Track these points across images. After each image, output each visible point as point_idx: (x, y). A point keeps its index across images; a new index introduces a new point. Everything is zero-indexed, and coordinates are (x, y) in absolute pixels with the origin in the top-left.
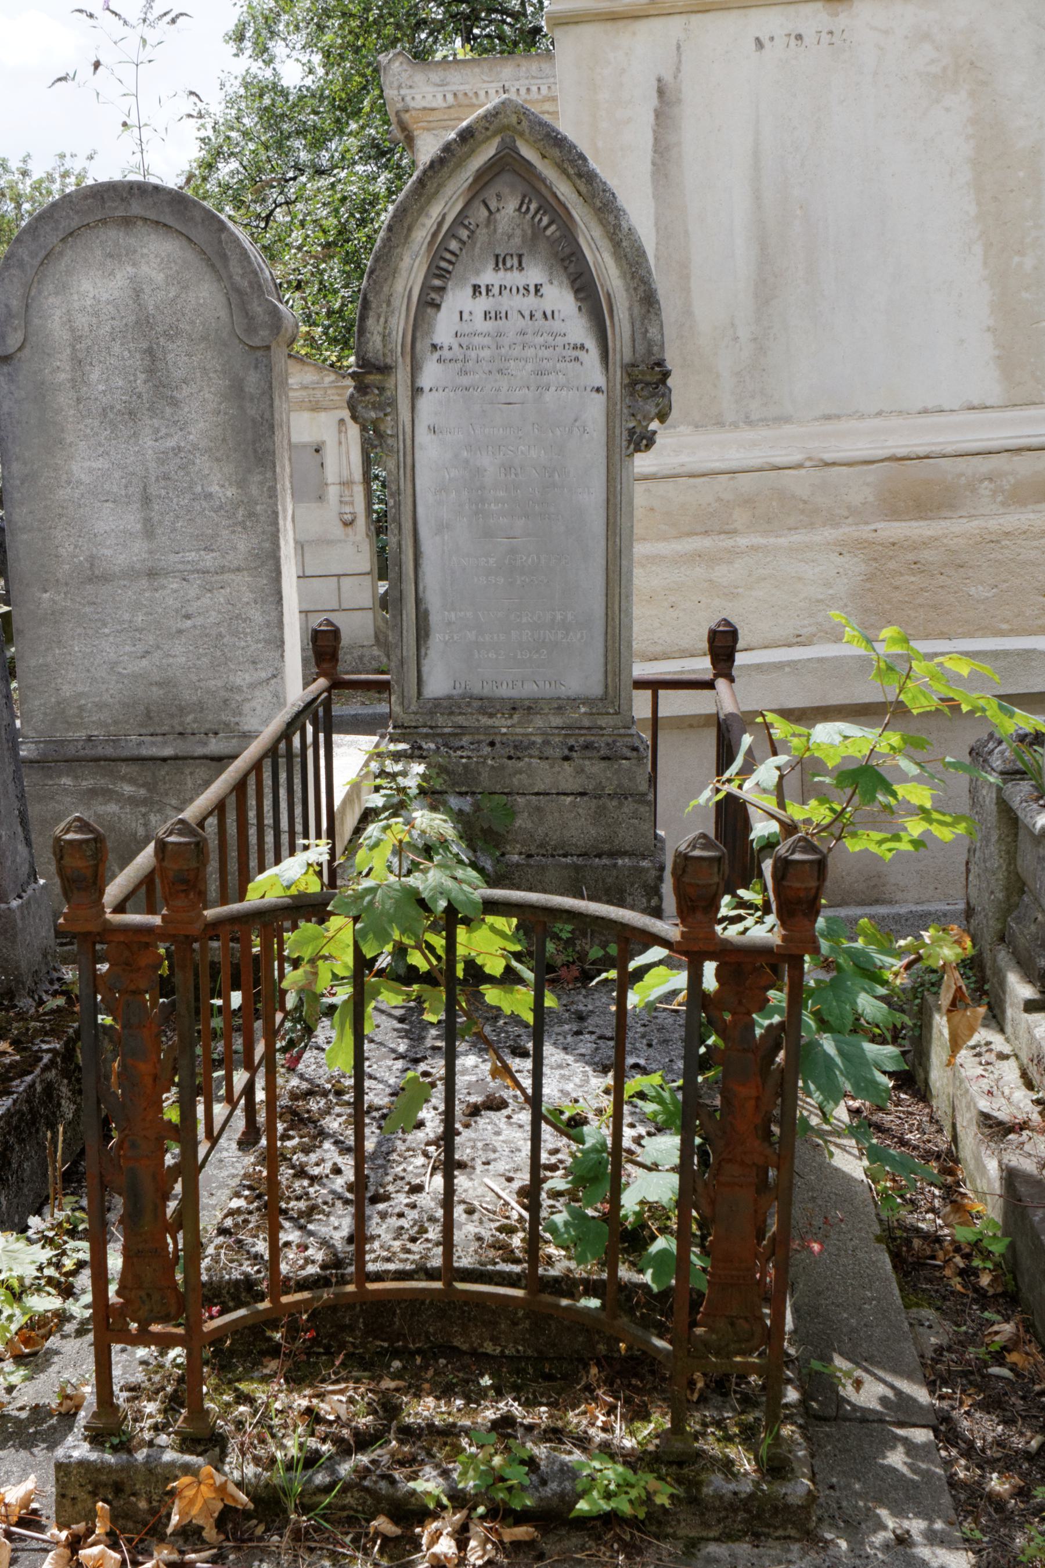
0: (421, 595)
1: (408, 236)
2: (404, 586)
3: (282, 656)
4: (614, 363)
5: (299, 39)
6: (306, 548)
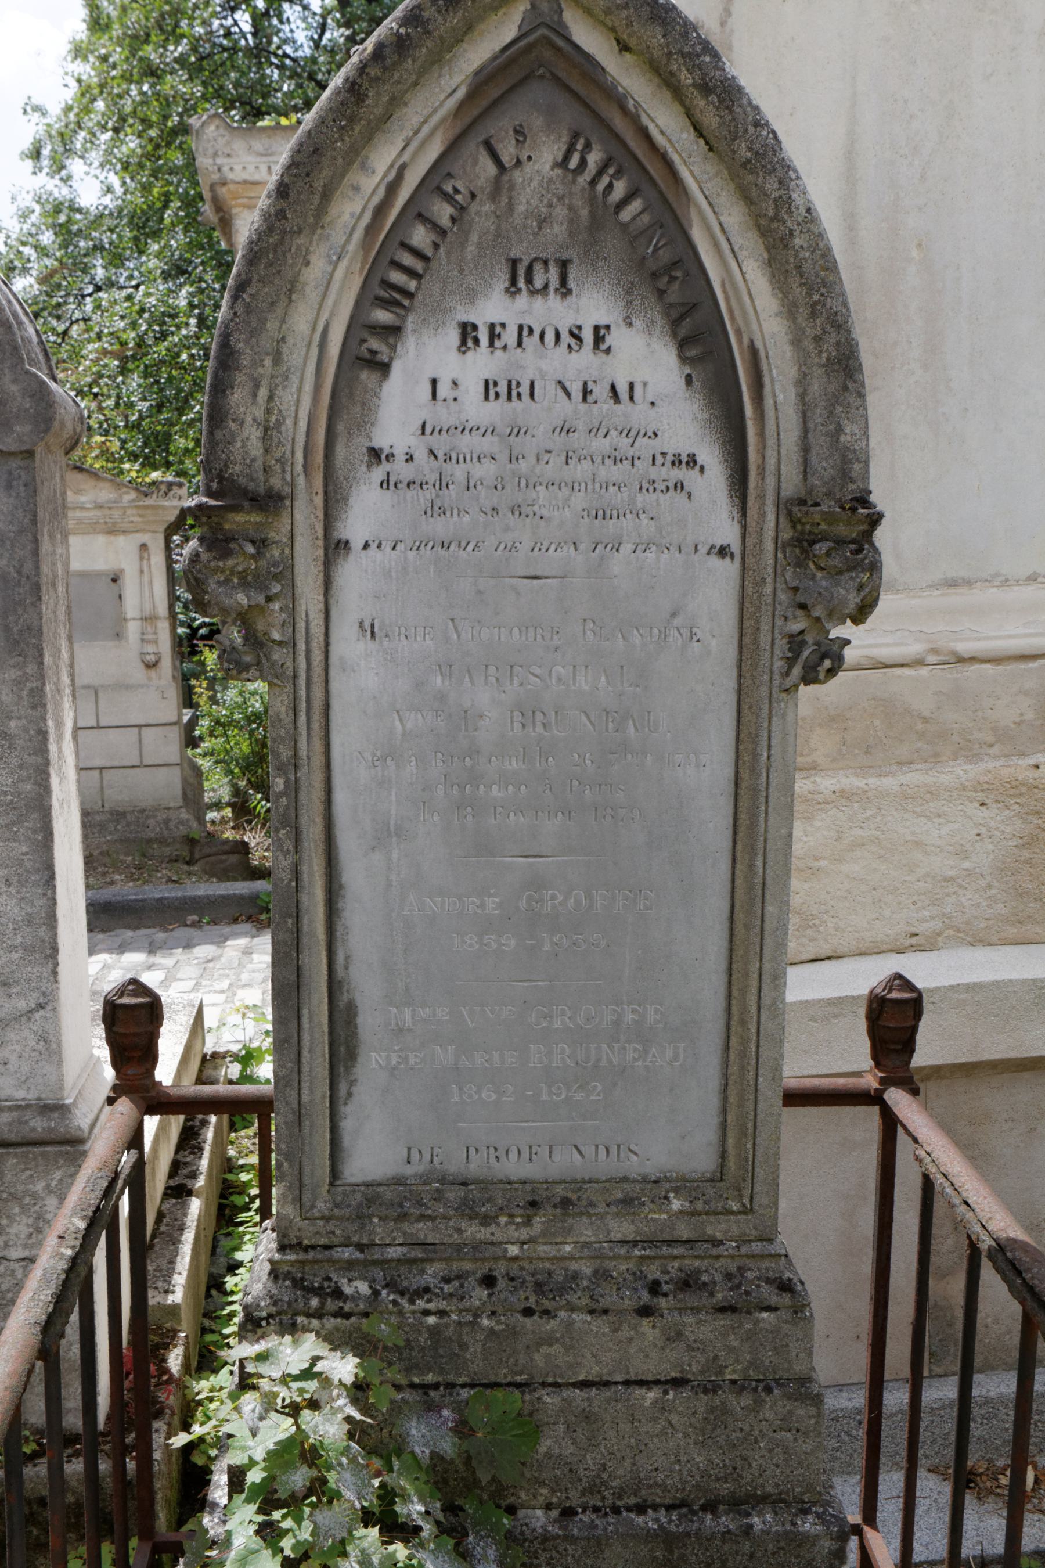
0: (340, 972)
1: (321, 211)
2: (305, 959)
3: (55, 973)
4: (761, 497)
5: (95, 156)
6: (100, 694)
